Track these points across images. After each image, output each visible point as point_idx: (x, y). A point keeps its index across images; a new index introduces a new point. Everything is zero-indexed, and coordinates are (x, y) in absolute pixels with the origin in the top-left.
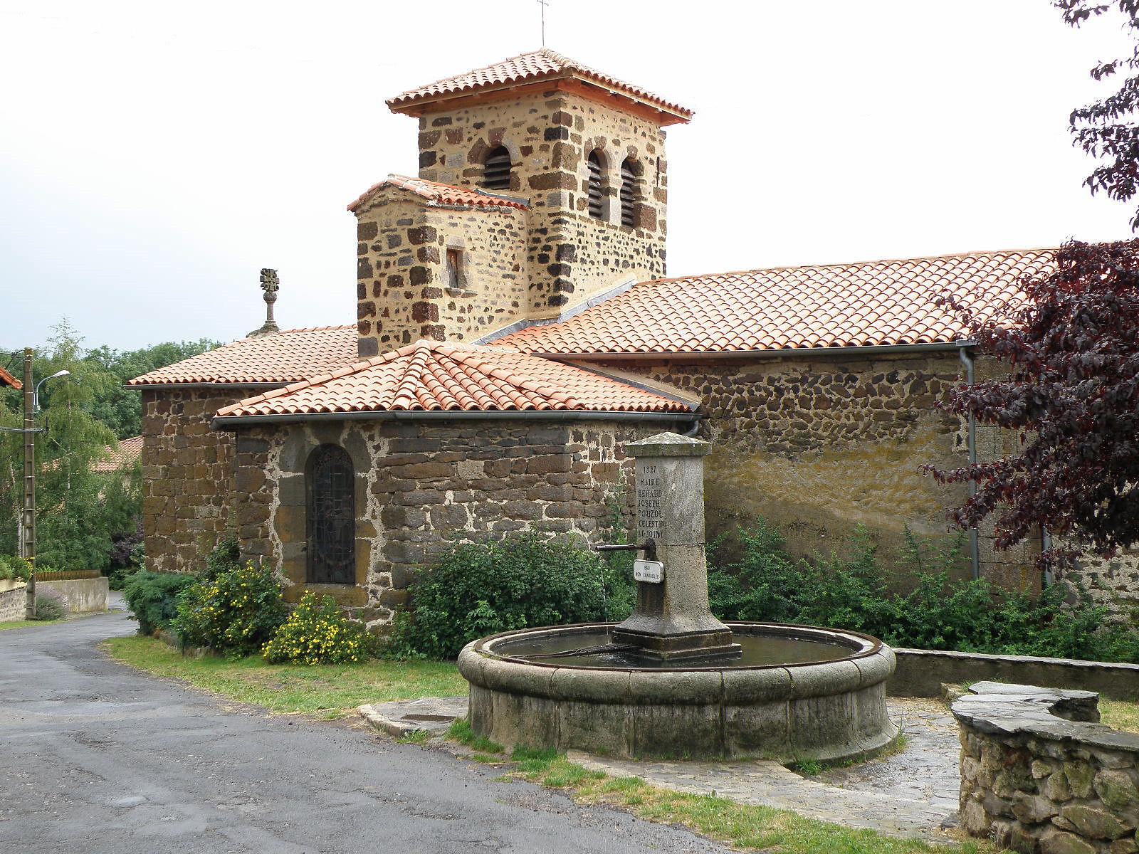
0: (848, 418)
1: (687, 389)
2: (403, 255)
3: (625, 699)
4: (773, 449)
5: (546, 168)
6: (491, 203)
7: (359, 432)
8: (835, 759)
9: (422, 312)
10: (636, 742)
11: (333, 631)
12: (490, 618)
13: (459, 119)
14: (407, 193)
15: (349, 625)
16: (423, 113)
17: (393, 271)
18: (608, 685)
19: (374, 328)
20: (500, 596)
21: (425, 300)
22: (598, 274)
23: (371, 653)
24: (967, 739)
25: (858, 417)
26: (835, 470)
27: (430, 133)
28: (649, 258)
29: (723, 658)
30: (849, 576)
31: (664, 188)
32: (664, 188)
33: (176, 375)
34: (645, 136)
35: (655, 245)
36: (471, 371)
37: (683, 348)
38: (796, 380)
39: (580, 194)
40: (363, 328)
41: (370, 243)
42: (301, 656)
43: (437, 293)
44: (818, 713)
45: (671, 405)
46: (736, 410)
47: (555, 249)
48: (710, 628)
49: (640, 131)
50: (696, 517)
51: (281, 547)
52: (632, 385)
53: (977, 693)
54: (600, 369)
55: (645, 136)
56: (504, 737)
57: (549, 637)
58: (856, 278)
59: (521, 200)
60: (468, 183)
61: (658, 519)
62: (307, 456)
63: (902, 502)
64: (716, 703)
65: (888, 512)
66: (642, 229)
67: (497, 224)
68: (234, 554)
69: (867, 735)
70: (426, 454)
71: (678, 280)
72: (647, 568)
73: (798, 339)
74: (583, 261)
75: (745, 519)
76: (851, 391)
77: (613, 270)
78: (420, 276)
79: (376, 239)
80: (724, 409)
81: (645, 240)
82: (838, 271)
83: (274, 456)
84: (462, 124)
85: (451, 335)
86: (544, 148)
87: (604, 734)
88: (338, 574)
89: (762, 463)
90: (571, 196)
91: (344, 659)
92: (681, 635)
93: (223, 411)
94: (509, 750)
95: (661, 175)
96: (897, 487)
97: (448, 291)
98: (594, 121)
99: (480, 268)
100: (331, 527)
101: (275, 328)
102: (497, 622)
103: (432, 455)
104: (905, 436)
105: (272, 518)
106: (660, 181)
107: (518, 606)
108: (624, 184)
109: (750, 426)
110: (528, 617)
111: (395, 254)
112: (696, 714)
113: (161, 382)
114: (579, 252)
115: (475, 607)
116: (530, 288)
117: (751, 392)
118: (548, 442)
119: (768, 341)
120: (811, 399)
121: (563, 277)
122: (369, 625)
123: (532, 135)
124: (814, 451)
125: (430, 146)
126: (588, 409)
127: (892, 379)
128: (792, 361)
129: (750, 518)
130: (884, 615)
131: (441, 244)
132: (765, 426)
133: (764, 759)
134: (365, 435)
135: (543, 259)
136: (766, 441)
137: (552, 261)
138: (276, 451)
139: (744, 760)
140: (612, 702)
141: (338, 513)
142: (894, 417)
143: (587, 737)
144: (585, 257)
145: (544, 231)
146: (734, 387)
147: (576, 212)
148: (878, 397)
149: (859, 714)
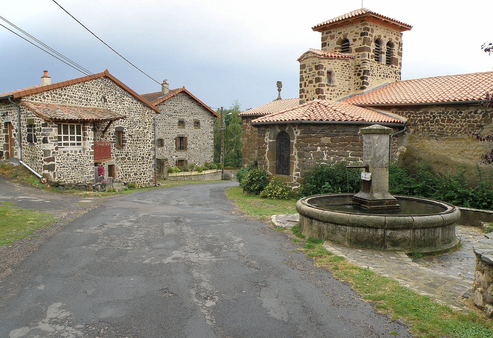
0: (458, 126)
1: (403, 116)
2: (313, 74)
3: (347, 224)
4: (431, 136)
5: (361, 45)
6: (342, 57)
7: (291, 128)
8: (429, 253)
9: (318, 91)
10: (351, 240)
11: (281, 189)
12: (329, 188)
13: (334, 32)
14: (315, 54)
15: (286, 188)
16: (323, 30)
17: (310, 79)
18: (341, 219)
19: (304, 97)
20: (333, 181)
21: (319, 88)
22: (377, 80)
23: (292, 197)
24: (478, 263)
25: (462, 126)
26: (452, 144)
27: (325, 37)
28: (395, 75)
29: (391, 209)
30: (454, 180)
31: (401, 52)
32: (401, 52)
33: (280, 118)
34: (395, 35)
35: (397, 70)
36: (338, 112)
37: (402, 102)
38: (441, 113)
39: (372, 53)
40: (301, 97)
41: (304, 70)
42: (270, 196)
43: (323, 85)
44: (424, 234)
45: (396, 121)
46: (419, 123)
47: (363, 71)
48: (388, 198)
49: (393, 33)
50: (385, 157)
51: (269, 163)
52: (384, 114)
53: (488, 238)
54: (374, 109)
55: (395, 35)
56: (306, 233)
57: (334, 197)
58: (463, 78)
59: (353, 56)
60: (336, 51)
61: (370, 157)
62: (277, 135)
63: (476, 155)
64: (382, 228)
65: (470, 159)
66: (393, 65)
67: (344, 64)
68: (256, 164)
69: (445, 243)
70: (312, 135)
71: (404, 81)
72: (366, 175)
73: (442, 99)
74: (372, 75)
75: (420, 159)
76: (460, 117)
77: (382, 78)
78: (318, 80)
79: (305, 69)
80: (415, 123)
81: (394, 69)
82: (459, 77)
83: (267, 135)
84: (335, 33)
85: (328, 99)
86: (360, 39)
87: (339, 236)
88: (285, 172)
89: (427, 141)
90: (369, 54)
91: (283, 198)
92: (376, 200)
93: (253, 121)
94: (307, 238)
95: (400, 47)
96: (474, 151)
97: (327, 85)
98: (377, 30)
99: (338, 77)
100: (283, 157)
101: (281, 99)
102: (331, 189)
103: (314, 135)
104: (478, 133)
105: (266, 154)
106: (400, 49)
107: (339, 185)
108: (387, 50)
109: (424, 128)
110: (342, 188)
111: (311, 73)
112: (374, 232)
113: (246, 114)
114: (371, 73)
115: (324, 184)
116: (355, 84)
117: (424, 117)
118: (352, 132)
119: (431, 99)
120: (445, 120)
121: (365, 80)
122: (293, 188)
123: (356, 35)
124: (446, 137)
125: (325, 41)
126: (366, 121)
127: (476, 112)
128: (439, 106)
129: (422, 159)
130: (465, 194)
131: (325, 70)
132: (429, 129)
133: (400, 251)
134: (293, 129)
135: (359, 75)
136: (429, 134)
137: (362, 75)
138: (268, 133)
139: (391, 251)
140: (342, 225)
141: (285, 153)
142: (475, 126)
143: (333, 237)
144: (373, 74)
145: (359, 66)
146: (419, 115)
147: (370, 59)
148: (470, 119)
149: (442, 235)
